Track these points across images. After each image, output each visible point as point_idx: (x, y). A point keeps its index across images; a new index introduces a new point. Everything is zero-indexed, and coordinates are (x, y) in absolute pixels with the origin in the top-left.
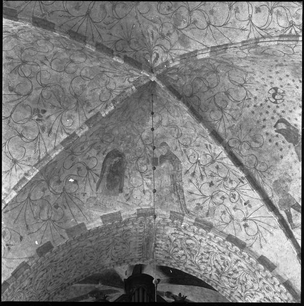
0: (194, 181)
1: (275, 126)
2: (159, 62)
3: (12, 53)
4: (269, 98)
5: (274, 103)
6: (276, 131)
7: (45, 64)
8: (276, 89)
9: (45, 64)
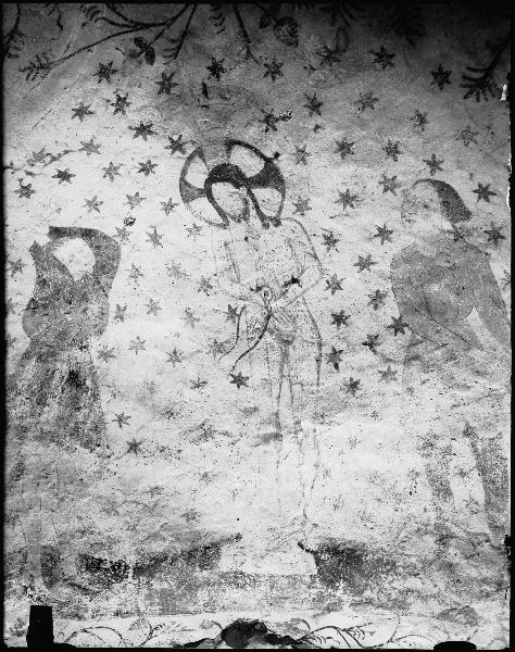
1: (57, 233)
5: (183, 183)
6: (35, 250)
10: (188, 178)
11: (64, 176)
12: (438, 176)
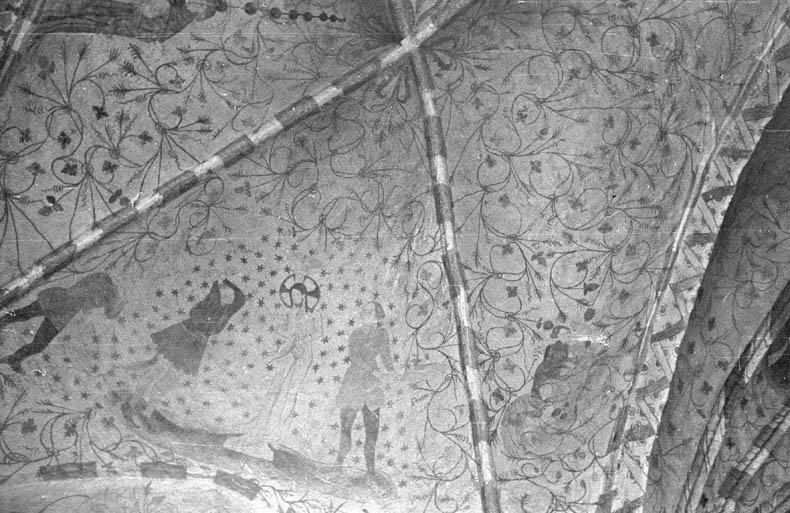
0: (114, 67)
1: (227, 282)
2: (434, 68)
3: (761, 284)
4: (294, 275)
5: (283, 286)
6: (215, 284)
8: (316, 293)
10: (286, 285)
11: (244, 261)
12: (377, 301)
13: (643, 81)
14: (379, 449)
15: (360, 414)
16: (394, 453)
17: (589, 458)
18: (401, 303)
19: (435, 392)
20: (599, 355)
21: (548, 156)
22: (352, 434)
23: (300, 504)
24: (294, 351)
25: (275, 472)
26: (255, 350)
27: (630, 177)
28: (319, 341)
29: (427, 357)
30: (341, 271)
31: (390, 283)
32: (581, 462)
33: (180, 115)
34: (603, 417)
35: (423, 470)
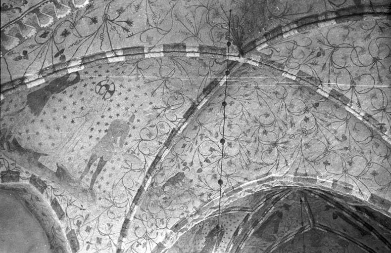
5: (100, 82)
7: (385, 24)
9: (385, 24)
12: (135, 114)
13: (289, 121)
14: (98, 179)
15: (99, 159)
16: (103, 183)
17: (164, 226)
18: (144, 122)
19: (132, 170)
20: (191, 189)
21: (239, 103)
22: (91, 167)
23: (59, 197)
24: (86, 116)
25: (56, 179)
26: (70, 108)
27: (253, 139)
28: (100, 116)
29: (138, 154)
30: (129, 90)
31: (145, 112)
32: (161, 225)
33: (120, 13)
34: (177, 213)
35: (110, 197)
